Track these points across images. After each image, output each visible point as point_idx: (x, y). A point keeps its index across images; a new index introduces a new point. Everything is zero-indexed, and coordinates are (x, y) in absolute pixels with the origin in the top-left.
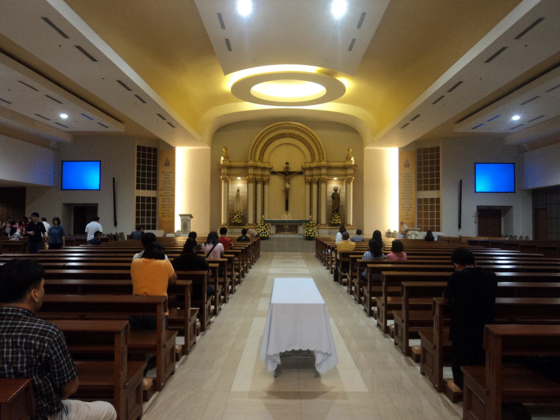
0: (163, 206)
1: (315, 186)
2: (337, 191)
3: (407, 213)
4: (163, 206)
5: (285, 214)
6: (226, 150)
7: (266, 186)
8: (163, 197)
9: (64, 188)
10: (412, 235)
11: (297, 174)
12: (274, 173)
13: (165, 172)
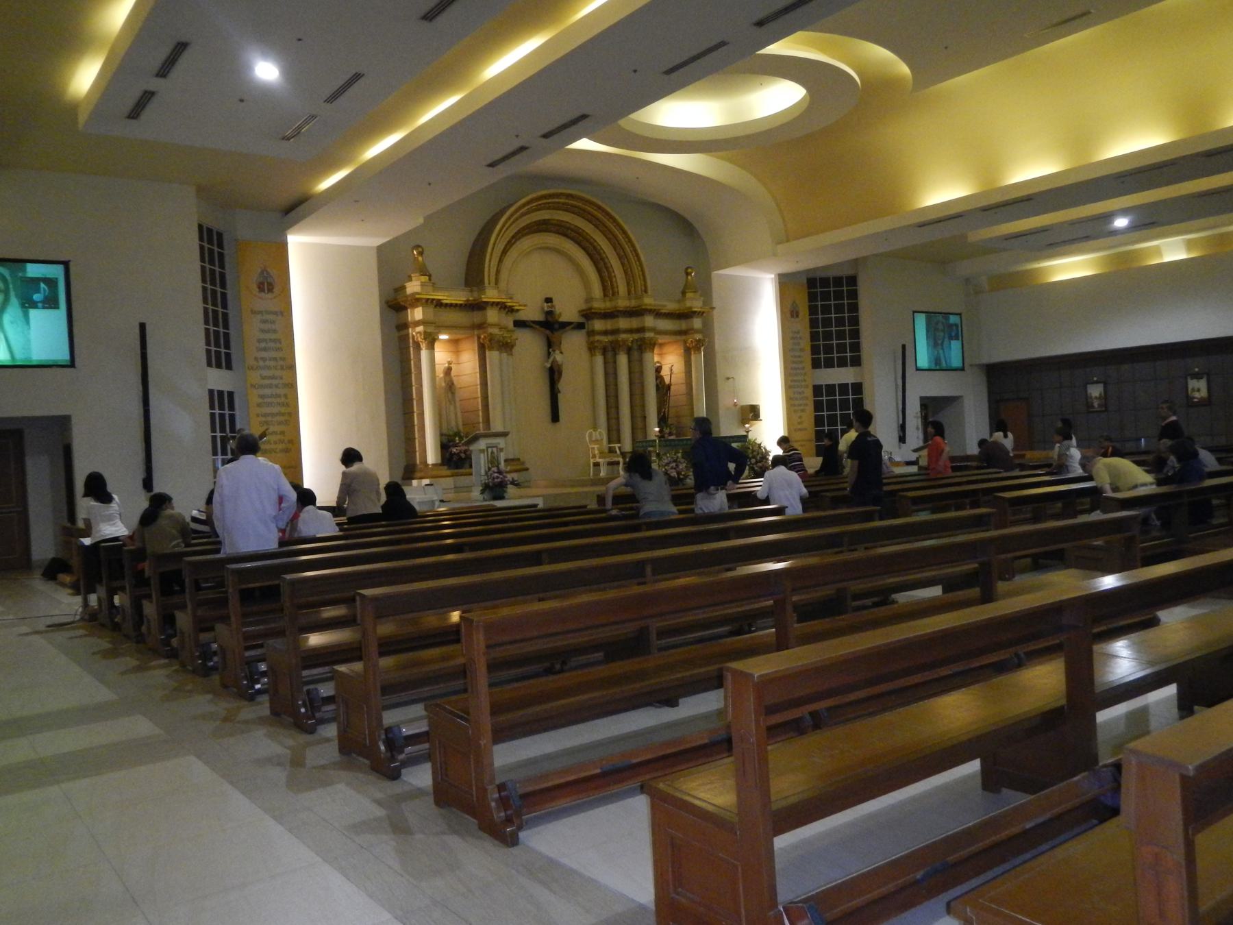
0: (264, 419)
1: (623, 360)
3: (800, 417)
4: (264, 419)
8: (262, 392)
9: (961, 365)
11: (574, 328)
12: (520, 324)
13: (261, 312)
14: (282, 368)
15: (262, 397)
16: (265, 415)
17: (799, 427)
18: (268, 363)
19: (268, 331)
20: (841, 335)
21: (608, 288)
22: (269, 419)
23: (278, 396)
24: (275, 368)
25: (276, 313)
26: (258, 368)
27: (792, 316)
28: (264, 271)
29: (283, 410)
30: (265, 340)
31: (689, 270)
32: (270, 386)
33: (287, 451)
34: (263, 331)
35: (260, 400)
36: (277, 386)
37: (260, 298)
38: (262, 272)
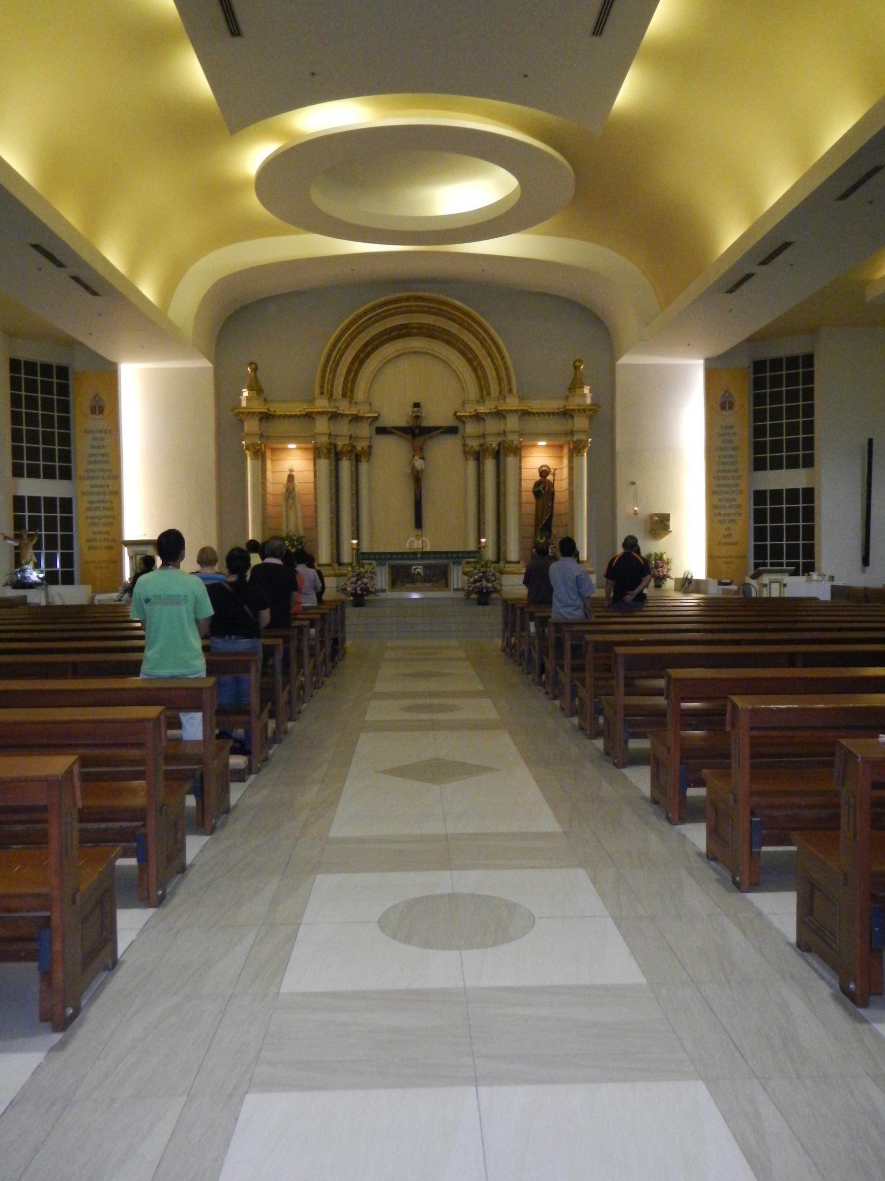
1: (489, 465)
2: (547, 474)
3: (729, 529)
5: (414, 538)
6: (255, 370)
7: (364, 466)
10: (773, 585)
11: (442, 433)
12: (382, 431)
13: (92, 432)
14: (109, 477)
15: (91, 502)
16: (92, 518)
17: (724, 540)
18: (96, 474)
19: (99, 447)
20: (776, 430)
21: (484, 391)
22: (97, 521)
23: (103, 501)
24: (103, 478)
25: (105, 432)
26: (88, 478)
27: (723, 407)
28: (96, 397)
29: (108, 513)
30: (95, 455)
31: (577, 364)
32: (98, 493)
33: (110, 548)
34: (93, 447)
35: (89, 505)
36: (104, 493)
37: (93, 419)
38: (95, 397)
